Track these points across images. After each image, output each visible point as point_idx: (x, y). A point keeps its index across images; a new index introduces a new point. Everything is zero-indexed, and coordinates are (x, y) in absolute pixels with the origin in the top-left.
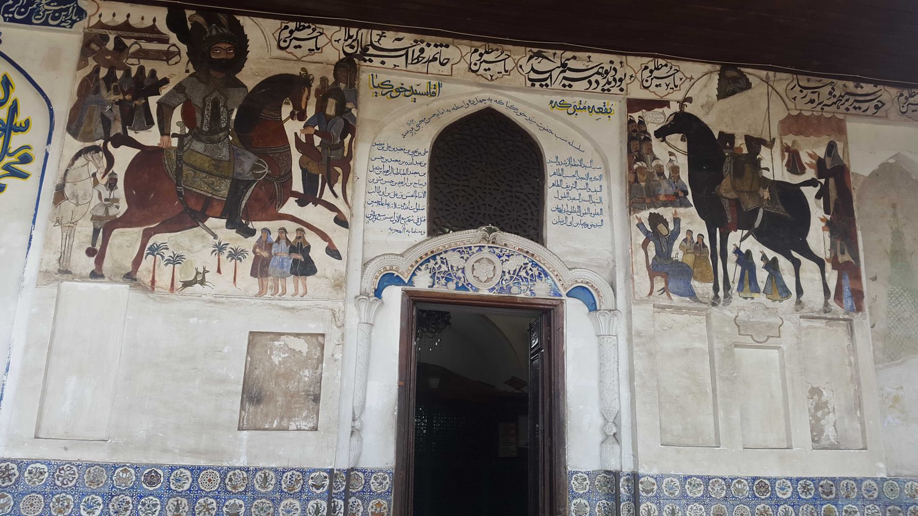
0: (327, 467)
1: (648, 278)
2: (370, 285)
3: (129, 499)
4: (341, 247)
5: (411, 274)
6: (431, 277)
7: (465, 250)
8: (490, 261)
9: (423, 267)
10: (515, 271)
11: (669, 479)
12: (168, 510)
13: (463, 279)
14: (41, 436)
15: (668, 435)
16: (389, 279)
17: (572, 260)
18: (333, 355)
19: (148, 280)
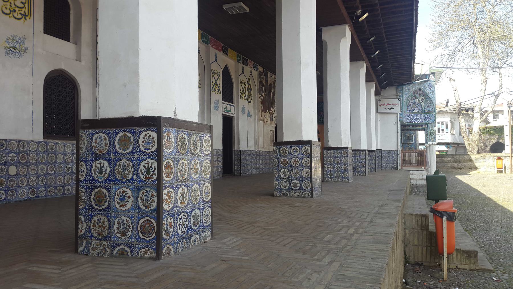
12: (140, 173)
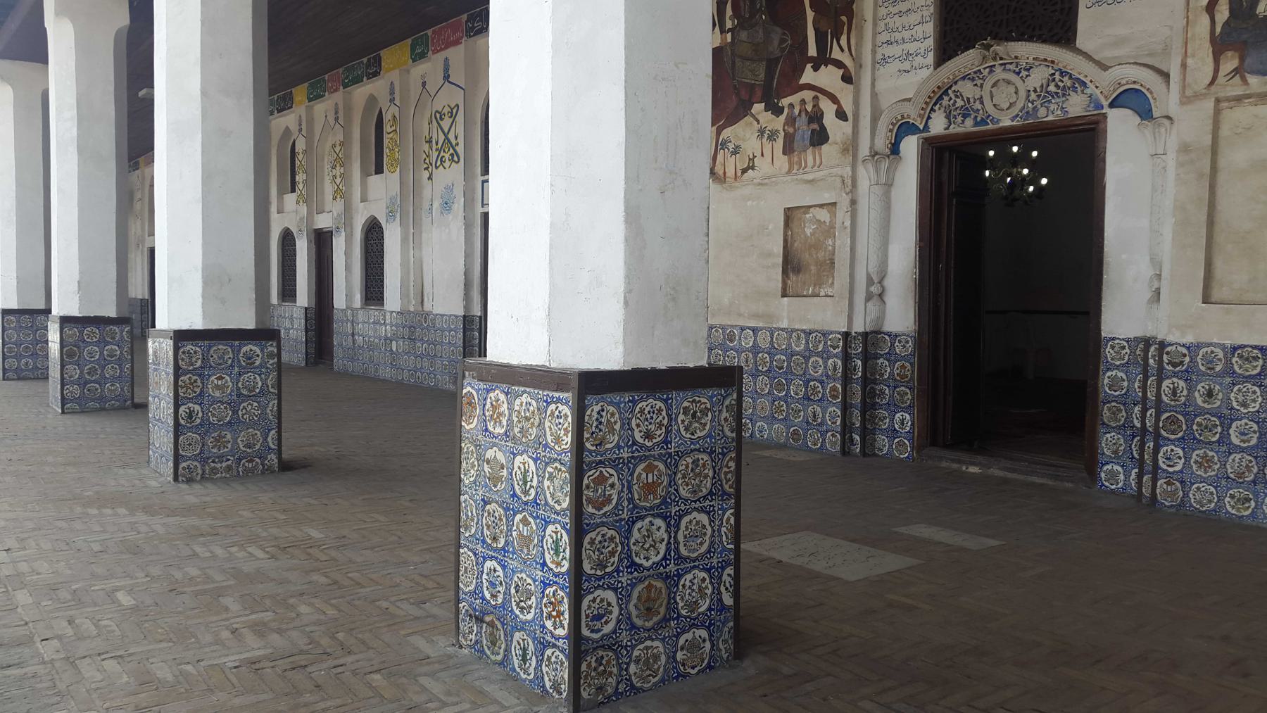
0: (841, 330)
1: (1210, 60)
2: (882, 143)
3: (720, 352)
4: (848, 108)
5: (925, 119)
6: (946, 117)
7: (975, 76)
8: (1009, 82)
9: (936, 108)
10: (1042, 86)
11: (1209, 350)
13: (981, 112)
14: (1213, 300)
15: (1224, 289)
16: (905, 129)
17: (1110, 56)
18: (843, 223)
19: (721, 173)
